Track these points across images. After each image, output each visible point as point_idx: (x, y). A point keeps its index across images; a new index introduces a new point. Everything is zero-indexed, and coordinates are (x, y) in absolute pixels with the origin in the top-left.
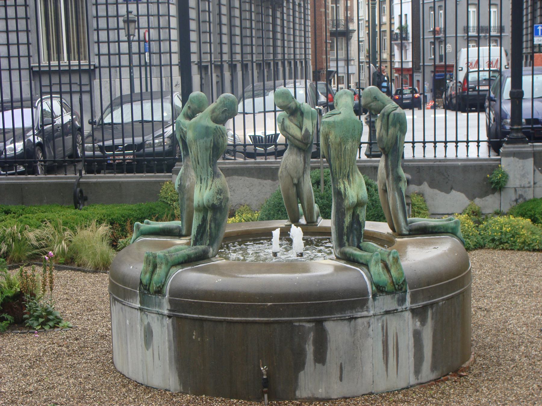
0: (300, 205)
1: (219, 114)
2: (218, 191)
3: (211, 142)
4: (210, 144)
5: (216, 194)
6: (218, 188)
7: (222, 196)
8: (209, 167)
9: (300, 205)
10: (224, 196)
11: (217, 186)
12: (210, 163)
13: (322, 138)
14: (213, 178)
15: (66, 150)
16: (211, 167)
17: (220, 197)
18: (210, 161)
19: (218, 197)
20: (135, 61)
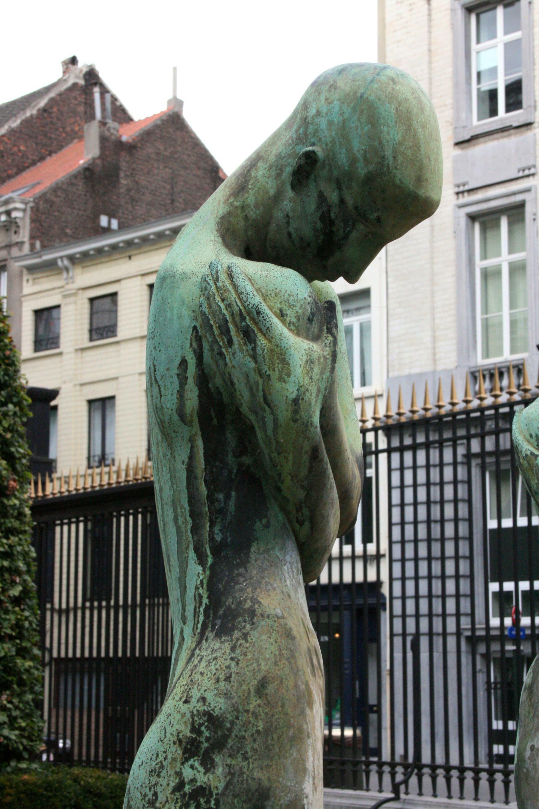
0: (148, 522)
1: (277, 198)
2: (195, 730)
3: (183, 380)
4: (181, 394)
5: (176, 752)
6: (195, 705)
7: (220, 770)
8: (192, 554)
9: (148, 522)
10: (231, 773)
11: (196, 694)
12: (196, 529)
13: (483, 746)
14: (202, 637)
15: (485, 674)
16: (201, 560)
17: (202, 779)
18: (194, 514)
19: (188, 773)
20: (423, 552)
